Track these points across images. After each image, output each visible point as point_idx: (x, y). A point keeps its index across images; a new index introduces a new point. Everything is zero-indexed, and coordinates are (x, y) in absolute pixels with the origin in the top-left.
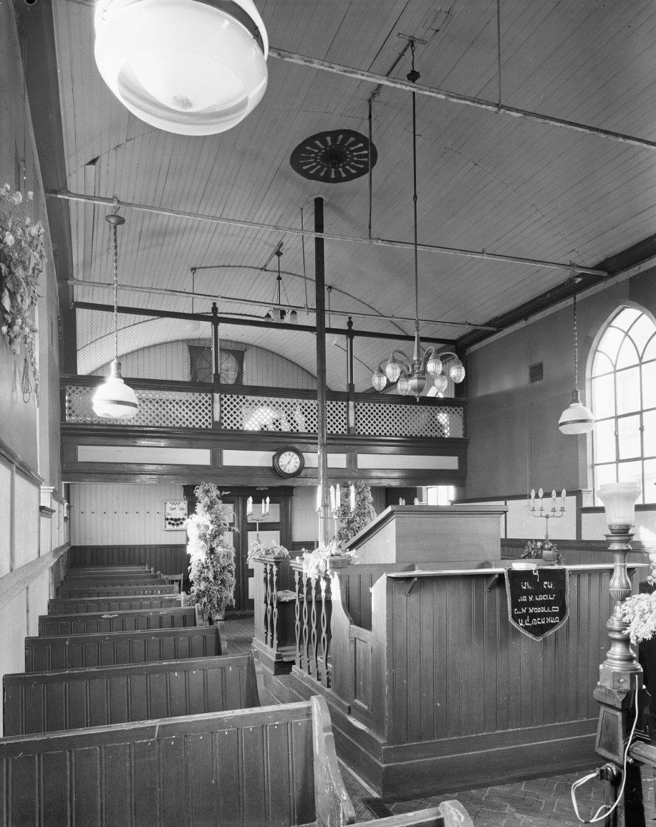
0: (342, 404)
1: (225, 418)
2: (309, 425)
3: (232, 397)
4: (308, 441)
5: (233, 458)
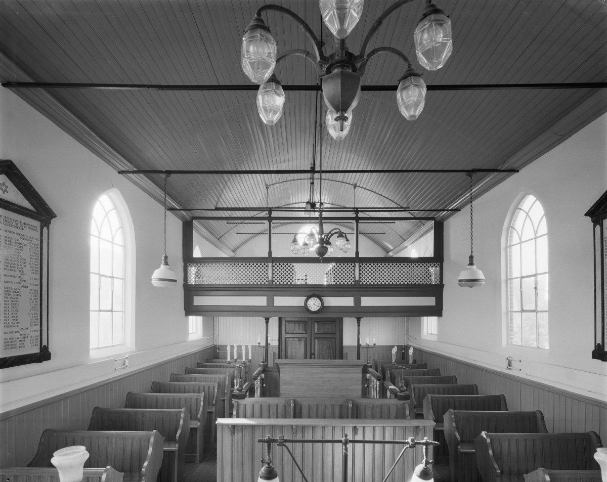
0: (351, 265)
1: (363, 278)
2: (291, 276)
3: (344, 265)
4: (260, 289)
5: (281, 301)
